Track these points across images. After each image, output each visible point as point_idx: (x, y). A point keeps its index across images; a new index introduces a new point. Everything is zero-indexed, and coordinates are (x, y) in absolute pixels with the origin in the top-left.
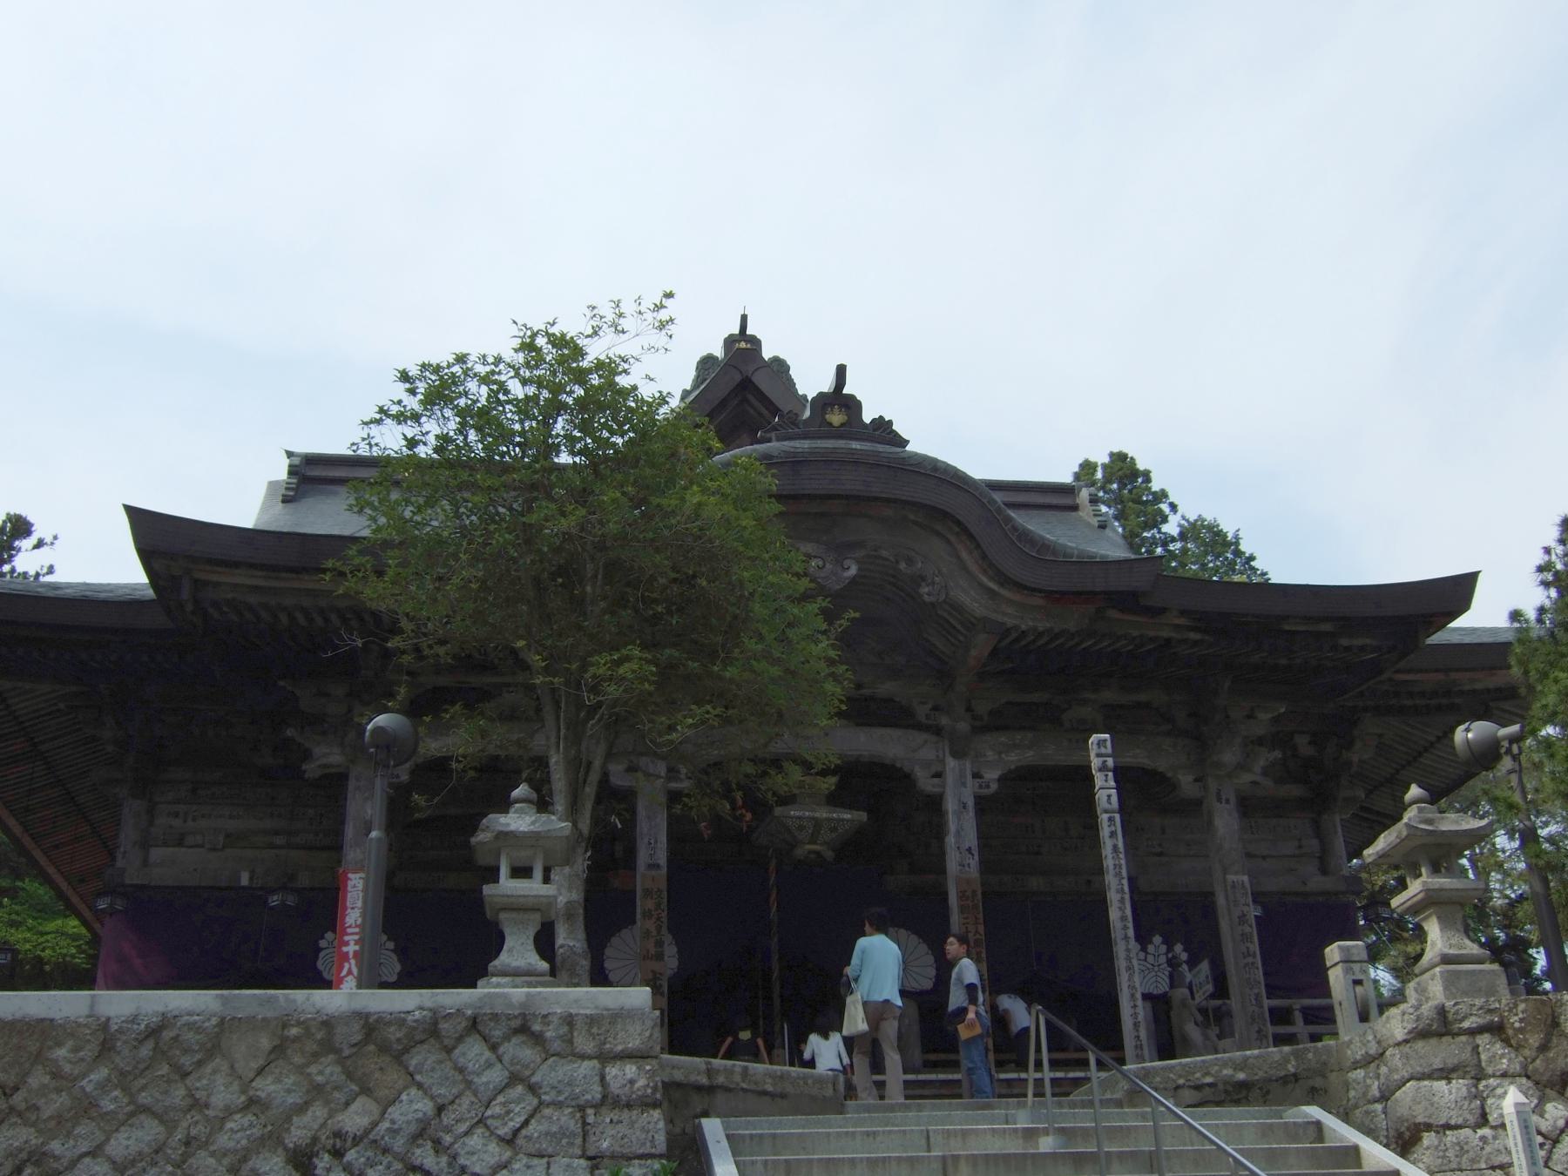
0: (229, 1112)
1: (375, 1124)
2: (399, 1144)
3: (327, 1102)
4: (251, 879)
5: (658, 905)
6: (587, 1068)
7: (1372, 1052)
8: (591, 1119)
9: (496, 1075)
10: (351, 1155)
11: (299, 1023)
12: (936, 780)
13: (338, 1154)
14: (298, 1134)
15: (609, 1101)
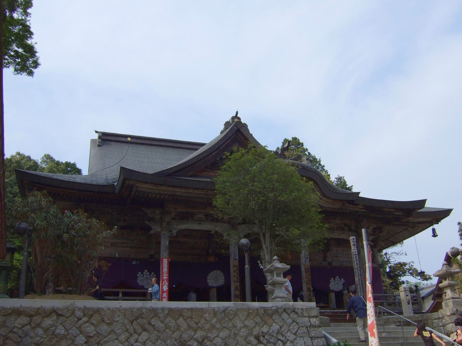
0: (241, 328)
1: (269, 330)
2: (275, 335)
3: (259, 326)
4: (119, 255)
5: (237, 269)
6: (307, 319)
7: (440, 317)
9: (290, 321)
10: (266, 337)
11: (251, 310)
13: (264, 336)
14: (255, 332)
15: (311, 326)
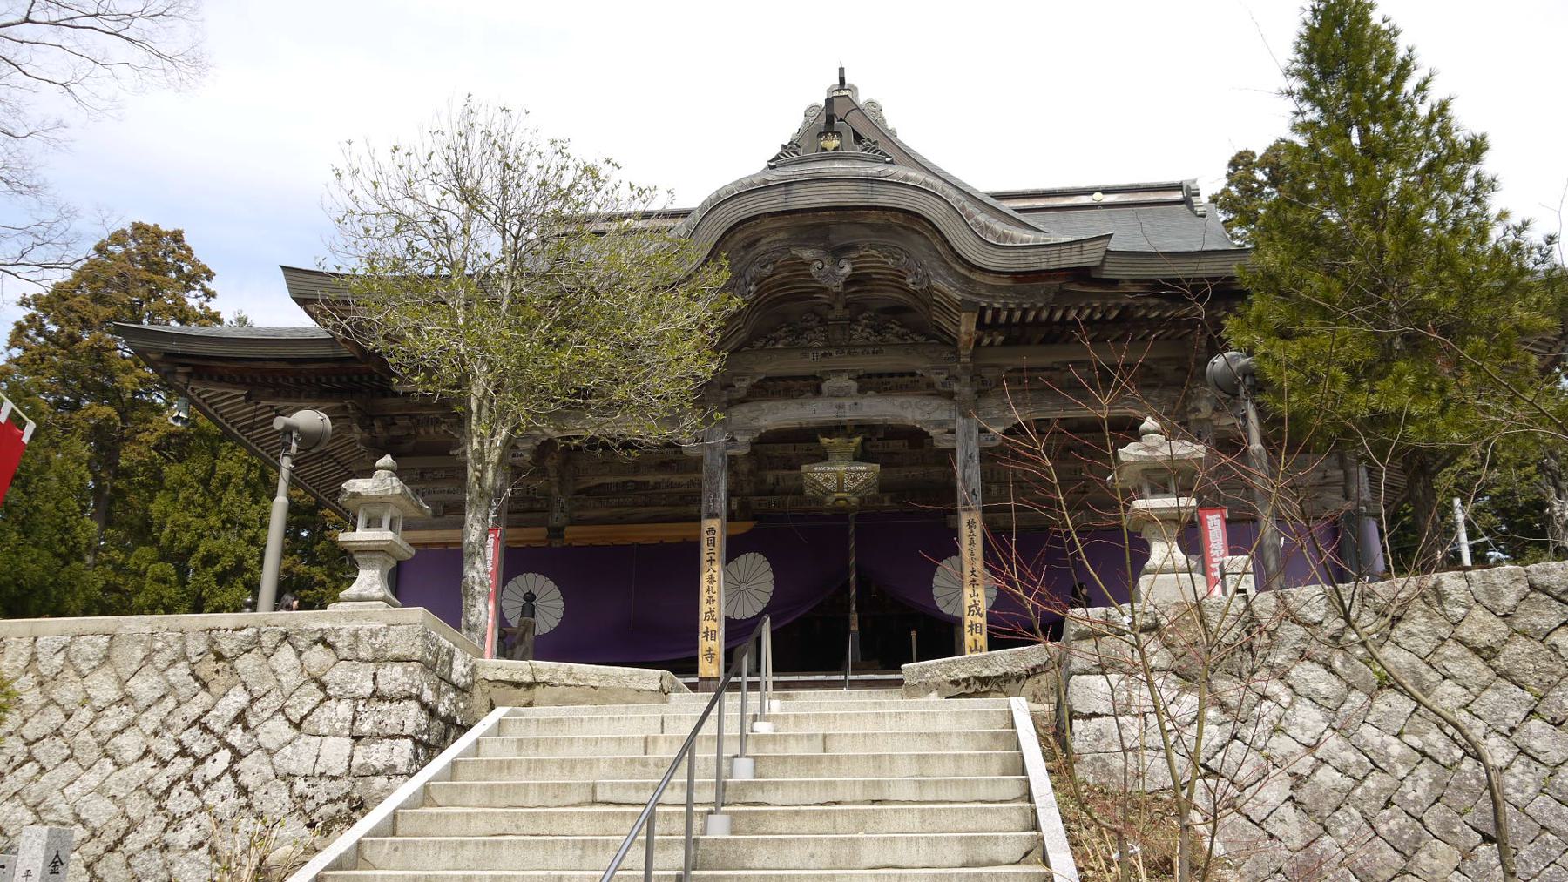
8: (360, 708)
12: (949, 437)
